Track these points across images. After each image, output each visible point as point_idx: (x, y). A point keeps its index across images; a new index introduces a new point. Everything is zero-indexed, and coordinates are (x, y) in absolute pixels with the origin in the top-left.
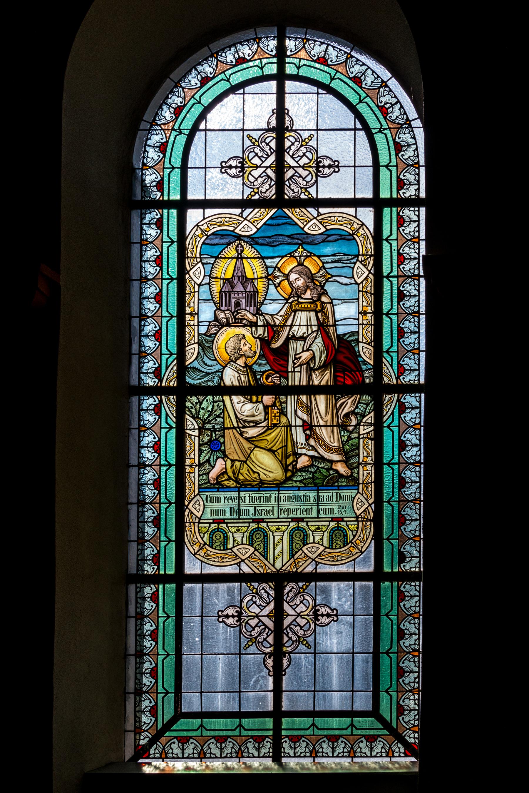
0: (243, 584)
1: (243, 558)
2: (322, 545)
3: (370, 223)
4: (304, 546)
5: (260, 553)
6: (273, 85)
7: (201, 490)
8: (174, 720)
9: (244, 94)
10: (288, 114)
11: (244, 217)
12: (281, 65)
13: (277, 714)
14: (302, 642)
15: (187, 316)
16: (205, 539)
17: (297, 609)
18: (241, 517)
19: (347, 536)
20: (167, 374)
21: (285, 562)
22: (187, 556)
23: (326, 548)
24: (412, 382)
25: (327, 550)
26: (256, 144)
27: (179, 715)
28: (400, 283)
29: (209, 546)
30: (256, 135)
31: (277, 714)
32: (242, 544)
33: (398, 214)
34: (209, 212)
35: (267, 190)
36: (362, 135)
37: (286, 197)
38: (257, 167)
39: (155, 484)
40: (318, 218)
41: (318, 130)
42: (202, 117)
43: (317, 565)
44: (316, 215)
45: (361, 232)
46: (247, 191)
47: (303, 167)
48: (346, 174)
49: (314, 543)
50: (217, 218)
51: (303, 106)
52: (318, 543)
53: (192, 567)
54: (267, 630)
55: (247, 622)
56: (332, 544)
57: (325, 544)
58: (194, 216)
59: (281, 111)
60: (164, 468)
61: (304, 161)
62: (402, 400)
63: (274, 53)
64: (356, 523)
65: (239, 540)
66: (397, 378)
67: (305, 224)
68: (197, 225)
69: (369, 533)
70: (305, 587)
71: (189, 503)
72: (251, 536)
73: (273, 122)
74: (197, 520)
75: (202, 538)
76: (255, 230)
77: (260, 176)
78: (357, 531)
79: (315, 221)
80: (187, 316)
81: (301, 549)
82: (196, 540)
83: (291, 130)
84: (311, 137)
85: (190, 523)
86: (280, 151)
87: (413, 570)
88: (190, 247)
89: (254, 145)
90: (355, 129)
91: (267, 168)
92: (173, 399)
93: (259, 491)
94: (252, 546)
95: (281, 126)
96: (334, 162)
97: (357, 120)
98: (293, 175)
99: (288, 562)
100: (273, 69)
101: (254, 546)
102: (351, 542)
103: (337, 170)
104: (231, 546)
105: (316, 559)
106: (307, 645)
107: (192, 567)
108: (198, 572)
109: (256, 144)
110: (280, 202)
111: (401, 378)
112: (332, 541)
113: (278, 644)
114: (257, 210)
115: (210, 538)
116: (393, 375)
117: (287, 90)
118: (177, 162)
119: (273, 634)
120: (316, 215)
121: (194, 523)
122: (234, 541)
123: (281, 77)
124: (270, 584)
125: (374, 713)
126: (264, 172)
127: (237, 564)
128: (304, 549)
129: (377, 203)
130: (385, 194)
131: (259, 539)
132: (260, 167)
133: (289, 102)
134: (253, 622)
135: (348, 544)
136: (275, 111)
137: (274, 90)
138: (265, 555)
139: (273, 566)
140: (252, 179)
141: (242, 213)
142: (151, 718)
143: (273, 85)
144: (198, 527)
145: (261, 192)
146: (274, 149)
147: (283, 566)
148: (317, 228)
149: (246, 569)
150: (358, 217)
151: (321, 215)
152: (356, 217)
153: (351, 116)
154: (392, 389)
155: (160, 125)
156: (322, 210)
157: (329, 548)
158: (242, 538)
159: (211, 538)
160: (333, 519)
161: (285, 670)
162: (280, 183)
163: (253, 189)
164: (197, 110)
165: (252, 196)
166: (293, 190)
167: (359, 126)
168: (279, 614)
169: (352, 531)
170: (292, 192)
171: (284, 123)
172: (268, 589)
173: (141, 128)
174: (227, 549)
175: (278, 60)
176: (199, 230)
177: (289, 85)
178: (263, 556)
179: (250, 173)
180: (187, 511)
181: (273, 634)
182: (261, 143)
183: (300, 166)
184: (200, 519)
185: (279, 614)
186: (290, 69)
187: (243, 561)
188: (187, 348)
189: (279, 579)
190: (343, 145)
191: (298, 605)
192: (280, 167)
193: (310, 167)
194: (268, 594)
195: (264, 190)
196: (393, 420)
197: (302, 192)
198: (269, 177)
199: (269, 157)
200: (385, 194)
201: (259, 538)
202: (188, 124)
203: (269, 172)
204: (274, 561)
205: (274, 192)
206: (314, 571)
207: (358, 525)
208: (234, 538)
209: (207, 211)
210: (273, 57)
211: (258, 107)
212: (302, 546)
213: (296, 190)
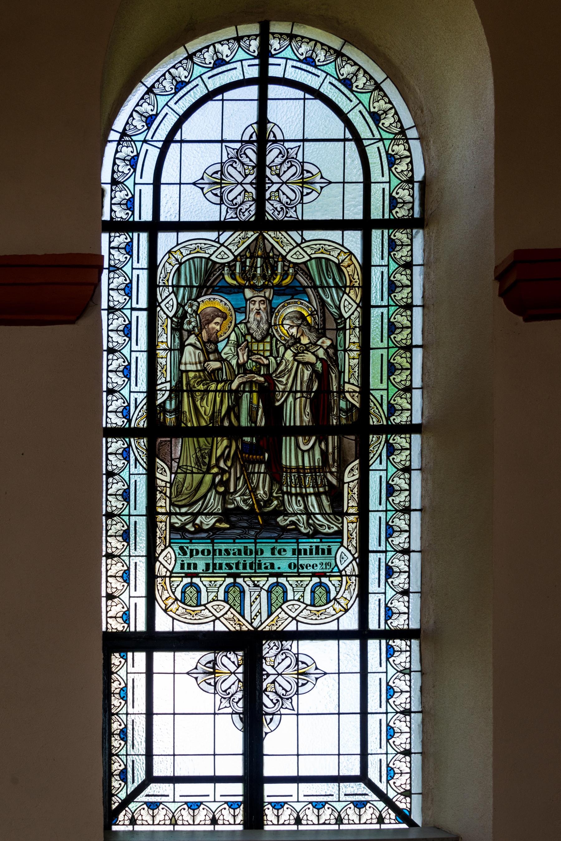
1: (298, 248)
2: (303, 603)
3: (357, 249)
4: (284, 603)
6: (253, 91)
7: (172, 541)
11: (221, 242)
12: (264, 67)
17: (242, 191)
18: (215, 571)
20: (381, 448)
22: (159, 612)
23: (307, 605)
24: (115, 440)
25: (308, 608)
27: (150, 778)
28: (127, 550)
29: (181, 601)
33: (389, 236)
34: (333, 626)
36: (351, 146)
39: (124, 536)
40: (302, 246)
42: (178, 126)
49: (294, 600)
52: (299, 600)
59: (263, 119)
62: (391, 441)
63: (256, 54)
66: (388, 419)
75: (173, 593)
81: (280, 607)
86: (261, 165)
87: (117, 234)
90: (345, 140)
92: (143, 442)
93: (234, 543)
94: (227, 603)
95: (262, 135)
97: (347, 130)
100: (254, 72)
102: (335, 599)
105: (218, 245)
110: (261, 223)
111: (392, 419)
113: (262, 154)
116: (383, 416)
117: (270, 95)
118: (149, 177)
123: (263, 81)
124: (270, 218)
128: (284, 607)
129: (365, 225)
130: (376, 214)
131: (234, 593)
135: (331, 601)
141: (218, 238)
142: (121, 782)
143: (253, 91)
150: (345, 245)
151: (306, 241)
152: (174, 619)
153: (341, 125)
154: (136, 433)
155: (130, 136)
157: (311, 605)
160: (314, 575)
162: (260, 201)
164: (172, 119)
167: (349, 135)
173: (110, 139)
174: (201, 605)
177: (273, 90)
184: (171, 572)
186: (274, 72)
187: (217, 618)
190: (332, 160)
192: (261, 184)
200: (376, 214)
202: (162, 134)
209: (335, 628)
210: (255, 58)
211: (239, 114)
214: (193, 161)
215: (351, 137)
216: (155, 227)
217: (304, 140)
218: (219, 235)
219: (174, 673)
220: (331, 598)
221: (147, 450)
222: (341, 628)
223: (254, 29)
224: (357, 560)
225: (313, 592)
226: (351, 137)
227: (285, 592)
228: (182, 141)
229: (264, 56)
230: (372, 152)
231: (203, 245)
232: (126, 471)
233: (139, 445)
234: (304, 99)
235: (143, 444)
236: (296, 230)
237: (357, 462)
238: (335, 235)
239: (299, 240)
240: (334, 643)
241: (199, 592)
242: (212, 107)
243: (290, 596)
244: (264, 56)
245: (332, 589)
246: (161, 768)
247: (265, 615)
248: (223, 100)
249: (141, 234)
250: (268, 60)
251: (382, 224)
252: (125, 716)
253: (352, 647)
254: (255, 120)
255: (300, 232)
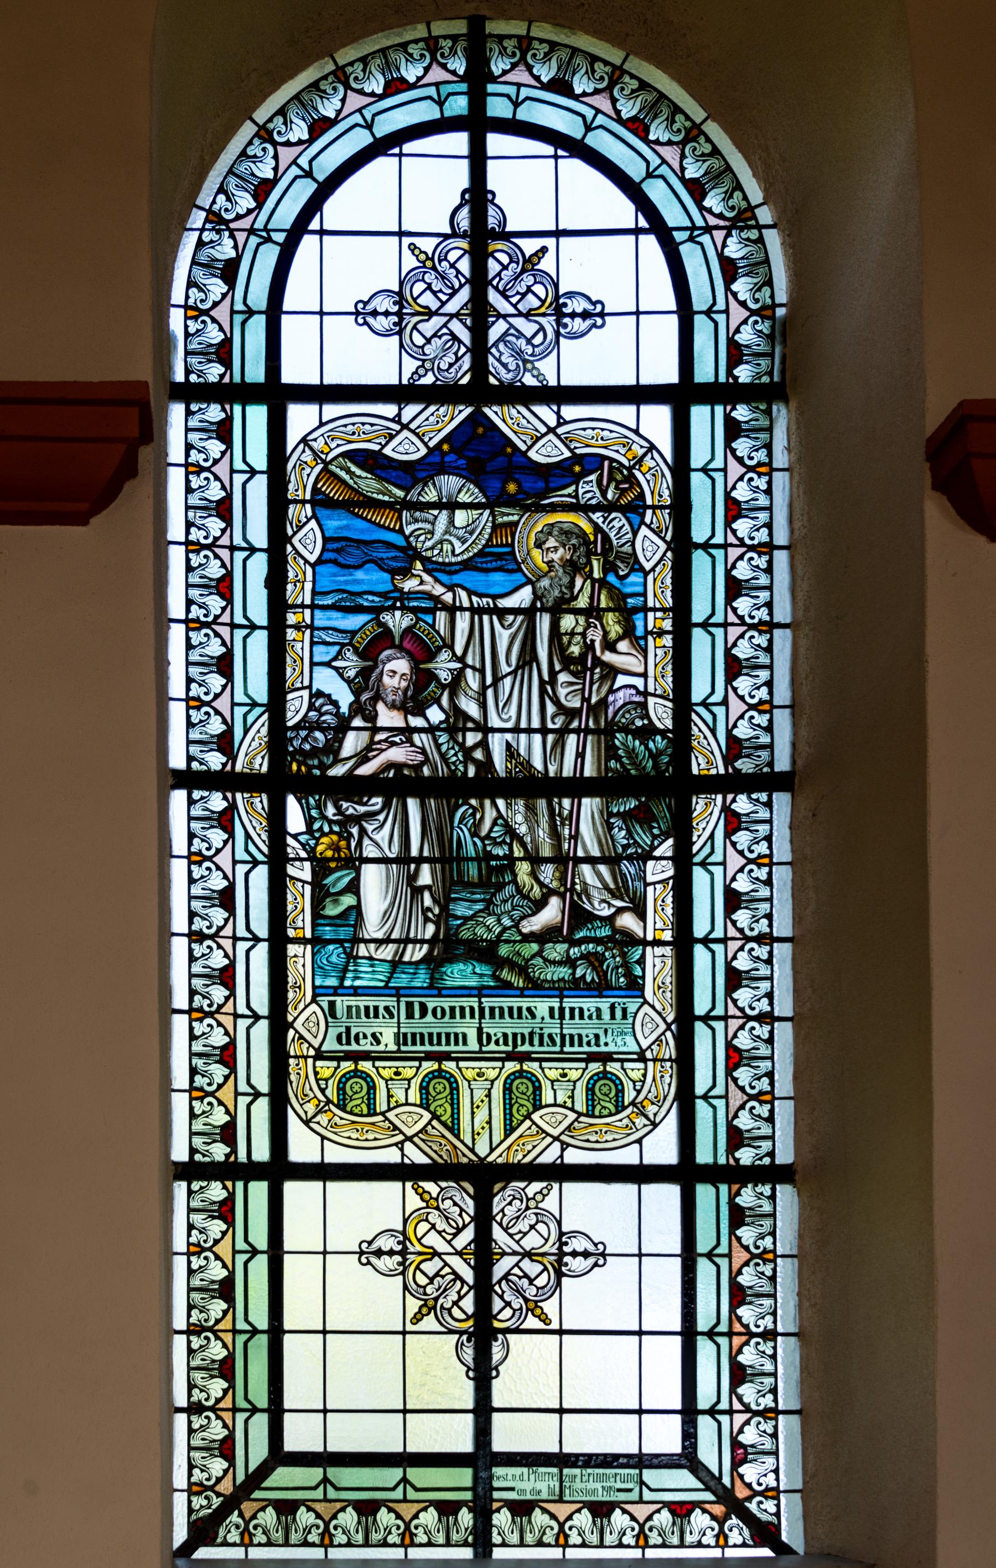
0: (553, 382)
2: (572, 1109)
5: (444, 1124)
6: (459, 142)
8: (265, 1470)
9: (401, 155)
10: (492, 202)
12: (478, 99)
13: (482, 1457)
14: (428, 258)
15: (289, 631)
16: (328, 1092)
19: (623, 1091)
21: (496, 1141)
23: (580, 1115)
25: (582, 1119)
26: (429, 264)
29: (337, 1106)
30: (427, 245)
31: (482, 1457)
32: (407, 1104)
34: (331, 411)
35: (451, 365)
36: (650, 243)
37: (492, 381)
38: (429, 313)
41: (404, 1333)
43: (563, 1150)
44: (408, 1145)
45: (648, 462)
46: (410, 365)
47: (435, 1254)
48: (346, 1236)
49: (555, 1105)
50: (614, 1140)
51: (526, 185)
52: (563, 1106)
53: (303, 1146)
54: (501, 287)
55: (543, 302)
56: (594, 1107)
57: (580, 1106)
58: (662, 1147)
59: (478, 195)
60: (242, 947)
61: (431, 1267)
64: (641, 1065)
65: (399, 1095)
67: (529, 443)
68: (655, 1125)
69: (670, 1085)
70: (539, 1197)
71: (664, 554)
72: (424, 1089)
73: (497, 1352)
74: (312, 1052)
75: (323, 1091)
76: (424, 451)
77: (435, 335)
78: (644, 1082)
79: (409, 1132)
80: (289, 631)
82: (648, 476)
83: (461, 1333)
84: (417, 1318)
85: (296, 1057)
88: (667, 1080)
89: (425, 267)
90: (637, 231)
91: (452, 316)
94: (427, 1109)
96: (369, 1263)
98: (455, 1235)
99: (502, 1142)
101: (432, 1108)
102: (633, 1103)
103: (599, 321)
104: (384, 1108)
106: (543, 1317)
107: (303, 1146)
108: (315, 1158)
109: (429, 264)
110: (480, 390)
112: (593, 1100)
113: (483, 1313)
114: (432, 408)
115: (338, 1089)
119: (472, 1293)
120: (408, 1145)
121: (306, 1057)
122: (390, 1096)
124: (466, 1185)
125: (279, 1456)
126: (445, 325)
127: (396, 1144)
128: (536, 1116)
132: (436, 313)
133: (496, 176)
134: (431, 1267)
135: (624, 1108)
136: (494, 1373)
137: (465, 151)
138: (454, 1129)
139: (472, 1150)
140: (419, 341)
141: (399, 415)
143: (459, 142)
144: (314, 1067)
145: (522, 1201)
146: (467, 275)
147: (492, 1150)
148: (404, 1117)
149: (547, 413)
150: (641, 431)
151: (566, 423)
154: (249, 783)
156: (569, 412)
157: (587, 1115)
158: (407, 1090)
159: (341, 1089)
161: (496, 1368)
163: (537, 1208)
165: (420, 377)
166: (455, 1204)
167: (643, 223)
168: (483, 1254)
169: (634, 1082)
170: (457, 1199)
171: (476, 1349)
172: (502, 371)
174: (375, 1114)
175: (469, 87)
176: (308, 452)
177: (496, 143)
178: (451, 1130)
179: (415, 327)
180: (668, 538)
181: (472, 1293)
182: (521, 1309)
183: (520, 314)
185: (483, 1254)
186: (498, 108)
188: (289, 696)
189: (484, 1178)
190: (614, 270)
191: (525, 1234)
193: (420, 1254)
194: (499, 360)
195: (444, 366)
196: (245, 716)
197: (437, 1199)
198: (455, 338)
199: (455, 292)
200: (259, 1190)
201: (440, 1093)
203: (456, 326)
204: (474, 1140)
205: (466, 366)
206: (559, 1161)
207: (646, 1069)
208: (388, 1090)
209: (326, 408)
211: (430, 183)
212: (531, 1109)
213: (448, 1203)
214: (347, 267)
215: (647, 226)
216: (686, 1173)
217: (558, 234)
218: (400, 409)
219: (325, 1253)
220: (626, 1103)
221: (691, 749)
222: (315, 408)
223: (460, 27)
224: (673, 1027)
225: (590, 1090)
226: (647, 226)
227: (538, 1089)
228: (322, 232)
229: (478, 80)
230: (691, 256)
231: (367, 427)
232: (206, 864)
233: (707, 758)
234: (556, 157)
235: (259, 806)
236: (414, 1166)
237: (670, 842)
238: (336, 1155)
239: (552, 422)
240: (331, 379)
241: (372, 1088)
242: (383, 166)
243: (547, 1097)
244: (478, 80)
245: (628, 1086)
246: (300, 1435)
247: (498, 1135)
248: (401, 155)
249: (710, 1160)
250: (485, 88)
251: (251, 1171)
252: (230, 1335)
253: (666, 1197)
254: (494, 1381)
255: (555, 408)
